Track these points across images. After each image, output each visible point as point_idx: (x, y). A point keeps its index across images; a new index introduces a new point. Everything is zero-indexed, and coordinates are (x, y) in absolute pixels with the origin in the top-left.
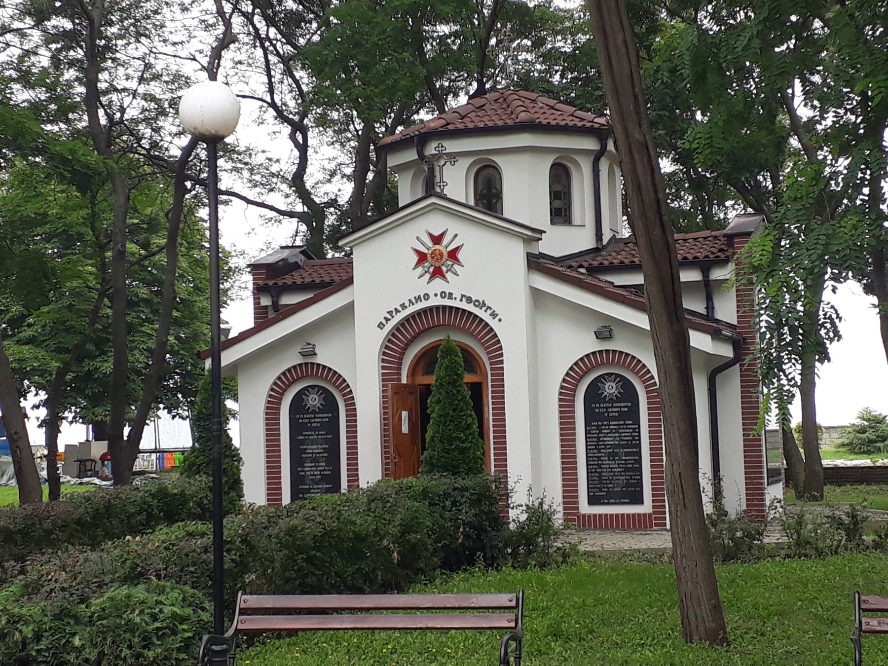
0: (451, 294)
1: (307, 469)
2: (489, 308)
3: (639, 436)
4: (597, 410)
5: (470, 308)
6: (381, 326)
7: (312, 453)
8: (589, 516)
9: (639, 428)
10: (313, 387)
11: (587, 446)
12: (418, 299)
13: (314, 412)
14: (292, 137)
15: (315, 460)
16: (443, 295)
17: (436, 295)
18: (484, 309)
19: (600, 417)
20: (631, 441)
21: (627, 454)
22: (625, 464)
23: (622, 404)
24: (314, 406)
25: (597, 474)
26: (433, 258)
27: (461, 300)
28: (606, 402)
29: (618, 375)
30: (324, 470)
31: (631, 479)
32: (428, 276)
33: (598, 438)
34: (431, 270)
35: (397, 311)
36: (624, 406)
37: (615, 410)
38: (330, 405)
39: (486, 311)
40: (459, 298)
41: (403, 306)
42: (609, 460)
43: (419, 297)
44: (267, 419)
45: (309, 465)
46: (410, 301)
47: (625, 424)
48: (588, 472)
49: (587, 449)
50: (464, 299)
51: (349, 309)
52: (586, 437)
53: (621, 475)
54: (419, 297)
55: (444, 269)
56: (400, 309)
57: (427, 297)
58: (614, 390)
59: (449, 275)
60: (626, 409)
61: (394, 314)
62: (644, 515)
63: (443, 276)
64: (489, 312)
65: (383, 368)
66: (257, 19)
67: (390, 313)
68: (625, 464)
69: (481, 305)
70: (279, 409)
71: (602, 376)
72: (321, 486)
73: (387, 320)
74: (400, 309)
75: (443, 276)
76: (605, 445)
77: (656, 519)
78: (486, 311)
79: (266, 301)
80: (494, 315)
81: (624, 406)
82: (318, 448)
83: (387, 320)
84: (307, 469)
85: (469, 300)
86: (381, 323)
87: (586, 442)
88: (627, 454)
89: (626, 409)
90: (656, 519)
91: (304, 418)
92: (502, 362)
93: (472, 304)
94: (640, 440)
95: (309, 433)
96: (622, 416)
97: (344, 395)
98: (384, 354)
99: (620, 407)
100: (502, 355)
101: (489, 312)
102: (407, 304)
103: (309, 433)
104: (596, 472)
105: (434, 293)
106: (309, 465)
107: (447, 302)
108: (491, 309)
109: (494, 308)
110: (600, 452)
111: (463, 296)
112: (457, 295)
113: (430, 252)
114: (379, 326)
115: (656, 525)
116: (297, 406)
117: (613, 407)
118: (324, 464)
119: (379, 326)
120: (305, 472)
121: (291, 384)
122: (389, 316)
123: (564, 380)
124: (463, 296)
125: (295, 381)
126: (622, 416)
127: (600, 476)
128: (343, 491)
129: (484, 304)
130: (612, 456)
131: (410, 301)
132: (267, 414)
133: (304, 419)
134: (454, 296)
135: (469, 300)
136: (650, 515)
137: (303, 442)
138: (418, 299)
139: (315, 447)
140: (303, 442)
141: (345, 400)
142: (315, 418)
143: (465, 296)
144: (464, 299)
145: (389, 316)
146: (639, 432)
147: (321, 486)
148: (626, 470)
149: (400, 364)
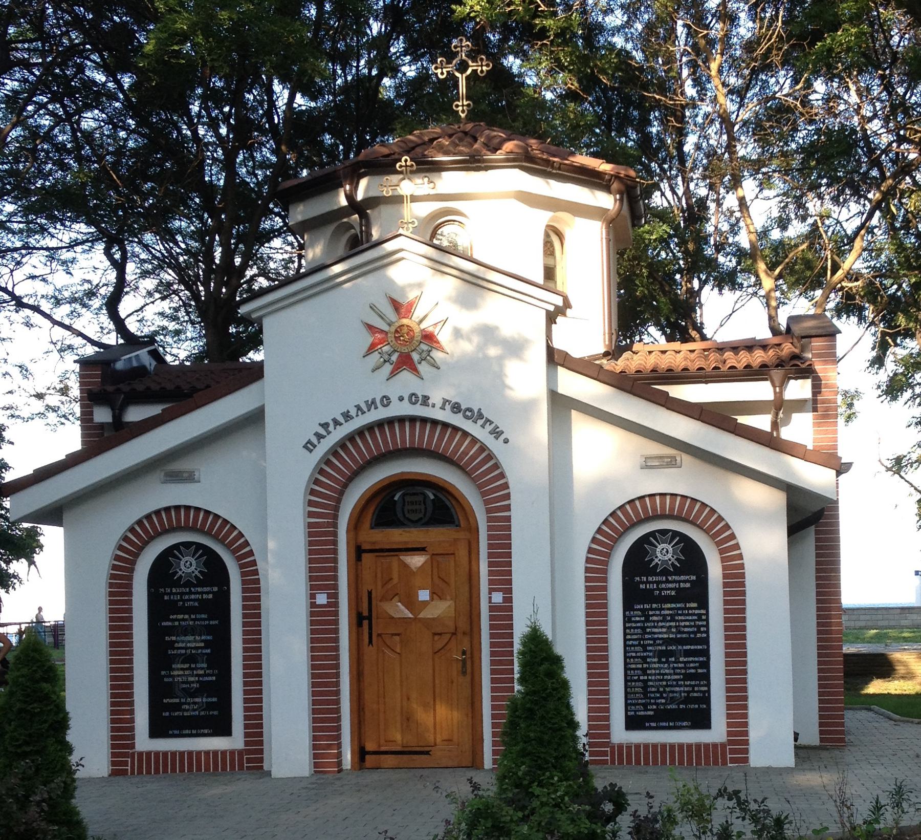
0: (426, 399)
1: (176, 673)
2: (487, 420)
3: (707, 626)
4: (642, 586)
5: (457, 420)
6: (309, 446)
7: (186, 648)
8: (629, 747)
9: (707, 614)
10: (187, 545)
11: (625, 640)
12: (371, 404)
13: (188, 584)
14: (108, 253)
15: (190, 659)
16: (413, 398)
17: (401, 399)
18: (480, 422)
19: (649, 597)
20: (695, 633)
21: (688, 653)
22: (685, 668)
23: (683, 578)
24: (189, 575)
25: (640, 684)
26: (397, 338)
27: (443, 408)
28: (656, 575)
29: (676, 534)
30: (205, 675)
31: (693, 691)
32: (388, 368)
33: (644, 629)
34: (394, 358)
35: (337, 423)
36: (685, 581)
37: (670, 586)
38: (215, 572)
39: (483, 426)
40: (439, 404)
41: (347, 416)
42: (660, 662)
43: (374, 402)
44: (111, 594)
45: (179, 666)
46: (358, 408)
47: (685, 608)
48: (626, 681)
49: (625, 646)
50: (448, 407)
51: (255, 419)
52: (625, 628)
53: (678, 685)
54: (374, 402)
55: (415, 357)
56: (341, 420)
57: (386, 401)
58: (670, 556)
59: (423, 368)
60: (688, 585)
61: (331, 428)
62: (715, 745)
63: (414, 370)
64: (489, 428)
65: (311, 514)
66: (32, 241)
67: (325, 426)
68: (685, 668)
69: (477, 416)
70: (130, 578)
71: (652, 534)
72: (197, 700)
73: (319, 437)
74: (341, 420)
75: (414, 370)
76: (655, 640)
77: (732, 751)
78: (483, 426)
79: (103, 415)
80: (497, 433)
81: (685, 581)
82: (195, 641)
83: (319, 437)
84: (176, 673)
85: (456, 408)
86: (309, 442)
87: (625, 634)
88: (688, 653)
89: (688, 585)
90: (732, 751)
91: (171, 594)
92: (508, 508)
93: (461, 415)
94: (707, 632)
95: (180, 617)
96: (682, 596)
97: (239, 559)
98: (313, 492)
99: (679, 582)
100: (508, 497)
101: (489, 428)
102: (353, 412)
103: (180, 617)
104: (639, 680)
105: (398, 395)
106: (179, 666)
107: (418, 411)
108: (491, 423)
109: (496, 422)
110: (645, 651)
111: (445, 401)
112: (436, 398)
113: (393, 329)
114: (305, 447)
115: (733, 760)
116: (162, 572)
117: (667, 581)
118: (205, 665)
119: (305, 447)
120: (173, 676)
121: (158, 535)
122: (322, 431)
123: (594, 540)
124: (445, 401)
125: (166, 532)
126: (682, 596)
127: (645, 687)
128: (486, 767)
129: (481, 416)
130: (664, 655)
131: (358, 408)
132: (111, 585)
133: (172, 594)
134: (430, 402)
135: (456, 408)
136: (723, 745)
137: (170, 631)
138: (371, 404)
139: (191, 638)
140: (170, 631)
141: (241, 566)
142: (191, 593)
143: (449, 402)
144: (448, 407)
145: (322, 431)
146: (707, 620)
147: (197, 700)
148: (687, 677)
149: (336, 509)
